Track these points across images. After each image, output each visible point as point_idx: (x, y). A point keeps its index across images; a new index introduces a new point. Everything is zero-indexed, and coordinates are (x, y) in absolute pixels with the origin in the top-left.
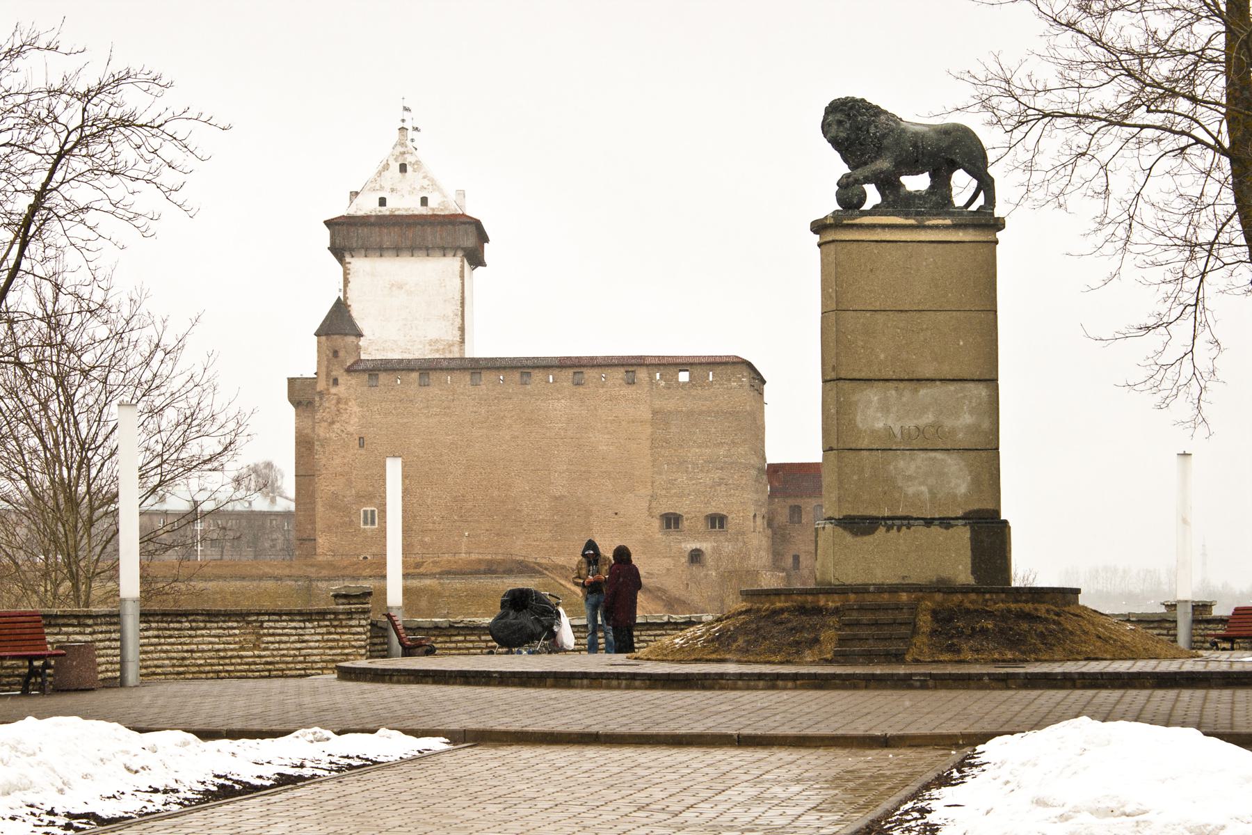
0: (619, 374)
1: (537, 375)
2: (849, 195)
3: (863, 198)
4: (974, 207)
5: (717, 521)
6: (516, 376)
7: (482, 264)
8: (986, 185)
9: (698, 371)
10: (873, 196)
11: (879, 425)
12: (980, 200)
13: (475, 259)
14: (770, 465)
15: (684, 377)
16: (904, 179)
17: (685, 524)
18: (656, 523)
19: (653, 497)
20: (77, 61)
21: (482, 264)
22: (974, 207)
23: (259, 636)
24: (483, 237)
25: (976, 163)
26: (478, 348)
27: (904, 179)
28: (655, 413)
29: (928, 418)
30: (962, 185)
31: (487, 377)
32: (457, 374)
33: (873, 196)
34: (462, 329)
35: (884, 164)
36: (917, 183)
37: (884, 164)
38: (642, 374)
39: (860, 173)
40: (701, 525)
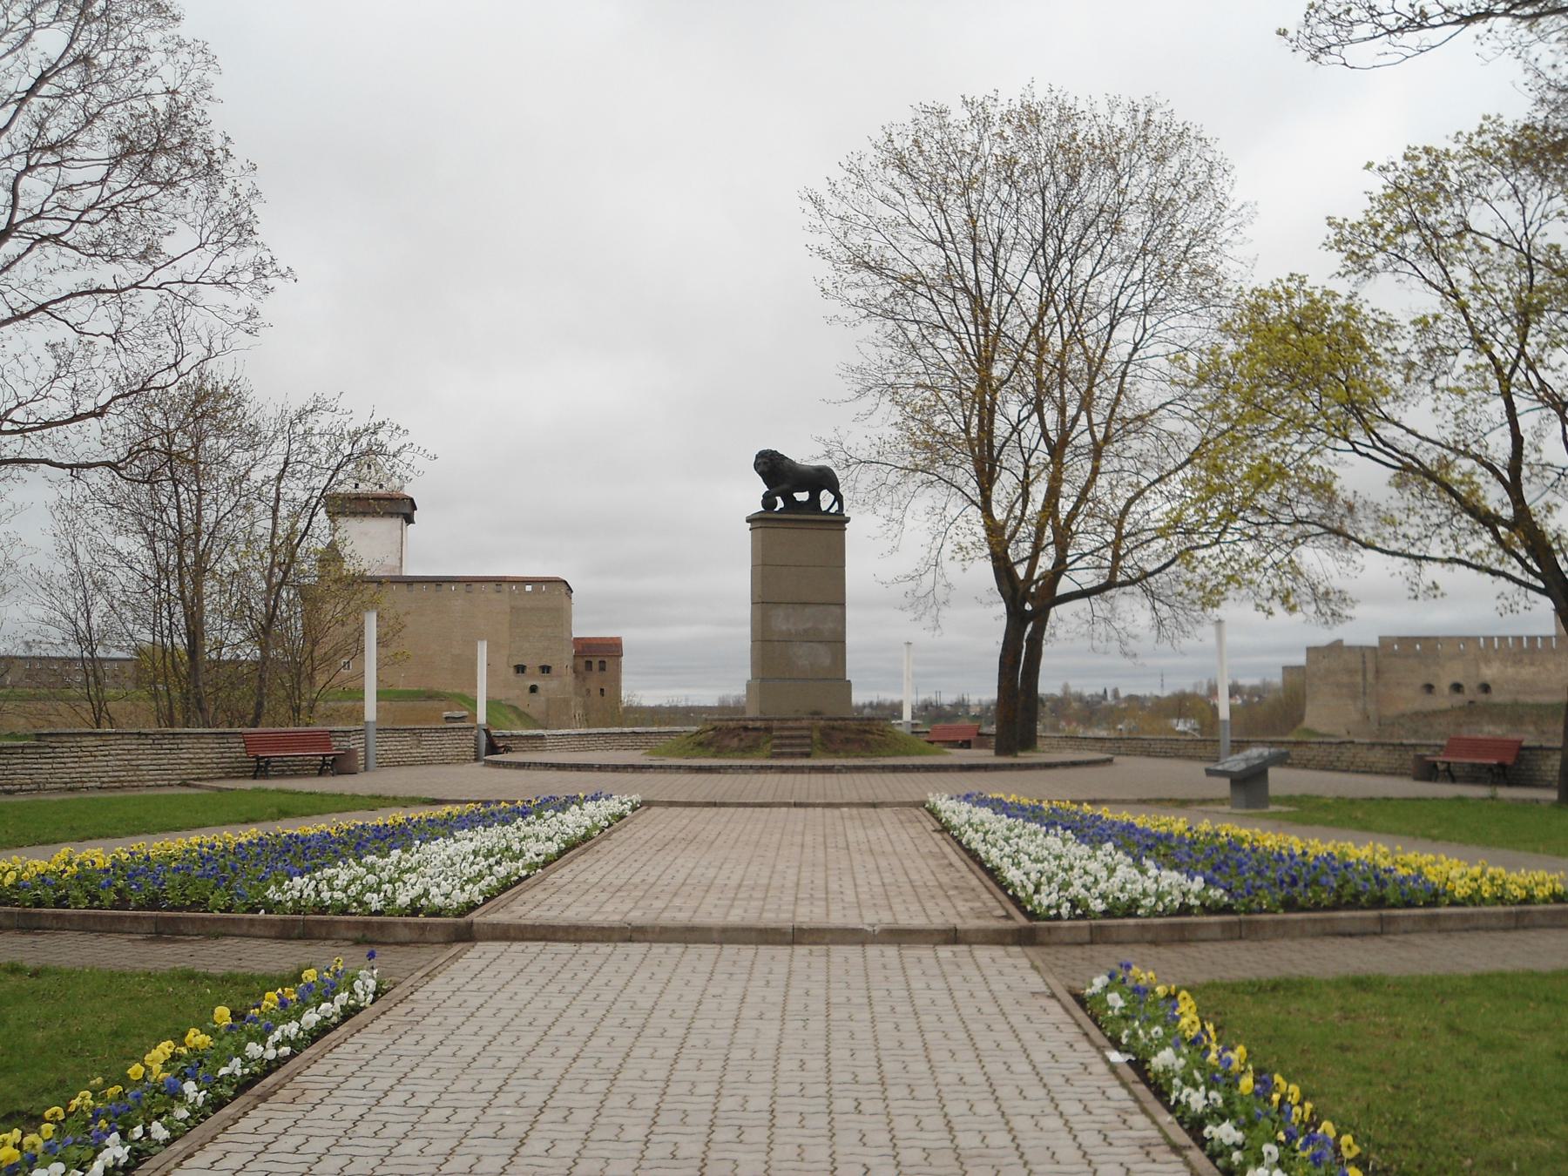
0: (493, 585)
1: (445, 586)
2: (768, 501)
3: (776, 503)
4: (832, 511)
5: (546, 669)
6: (434, 585)
7: (413, 522)
8: (839, 498)
9: (536, 585)
10: (780, 504)
11: (784, 628)
12: (836, 507)
13: (409, 519)
14: (576, 639)
15: (529, 588)
16: (795, 495)
17: (527, 671)
18: (512, 670)
19: (509, 656)
20: (346, 418)
21: (413, 522)
22: (832, 511)
23: (420, 741)
24: (414, 508)
25: (833, 486)
26: (410, 570)
27: (795, 495)
28: (512, 608)
29: (809, 625)
30: (826, 499)
31: (415, 586)
32: (400, 585)
33: (780, 504)
34: (401, 559)
35: (785, 486)
36: (802, 497)
37: (785, 486)
38: (505, 586)
39: (773, 491)
40: (538, 672)
